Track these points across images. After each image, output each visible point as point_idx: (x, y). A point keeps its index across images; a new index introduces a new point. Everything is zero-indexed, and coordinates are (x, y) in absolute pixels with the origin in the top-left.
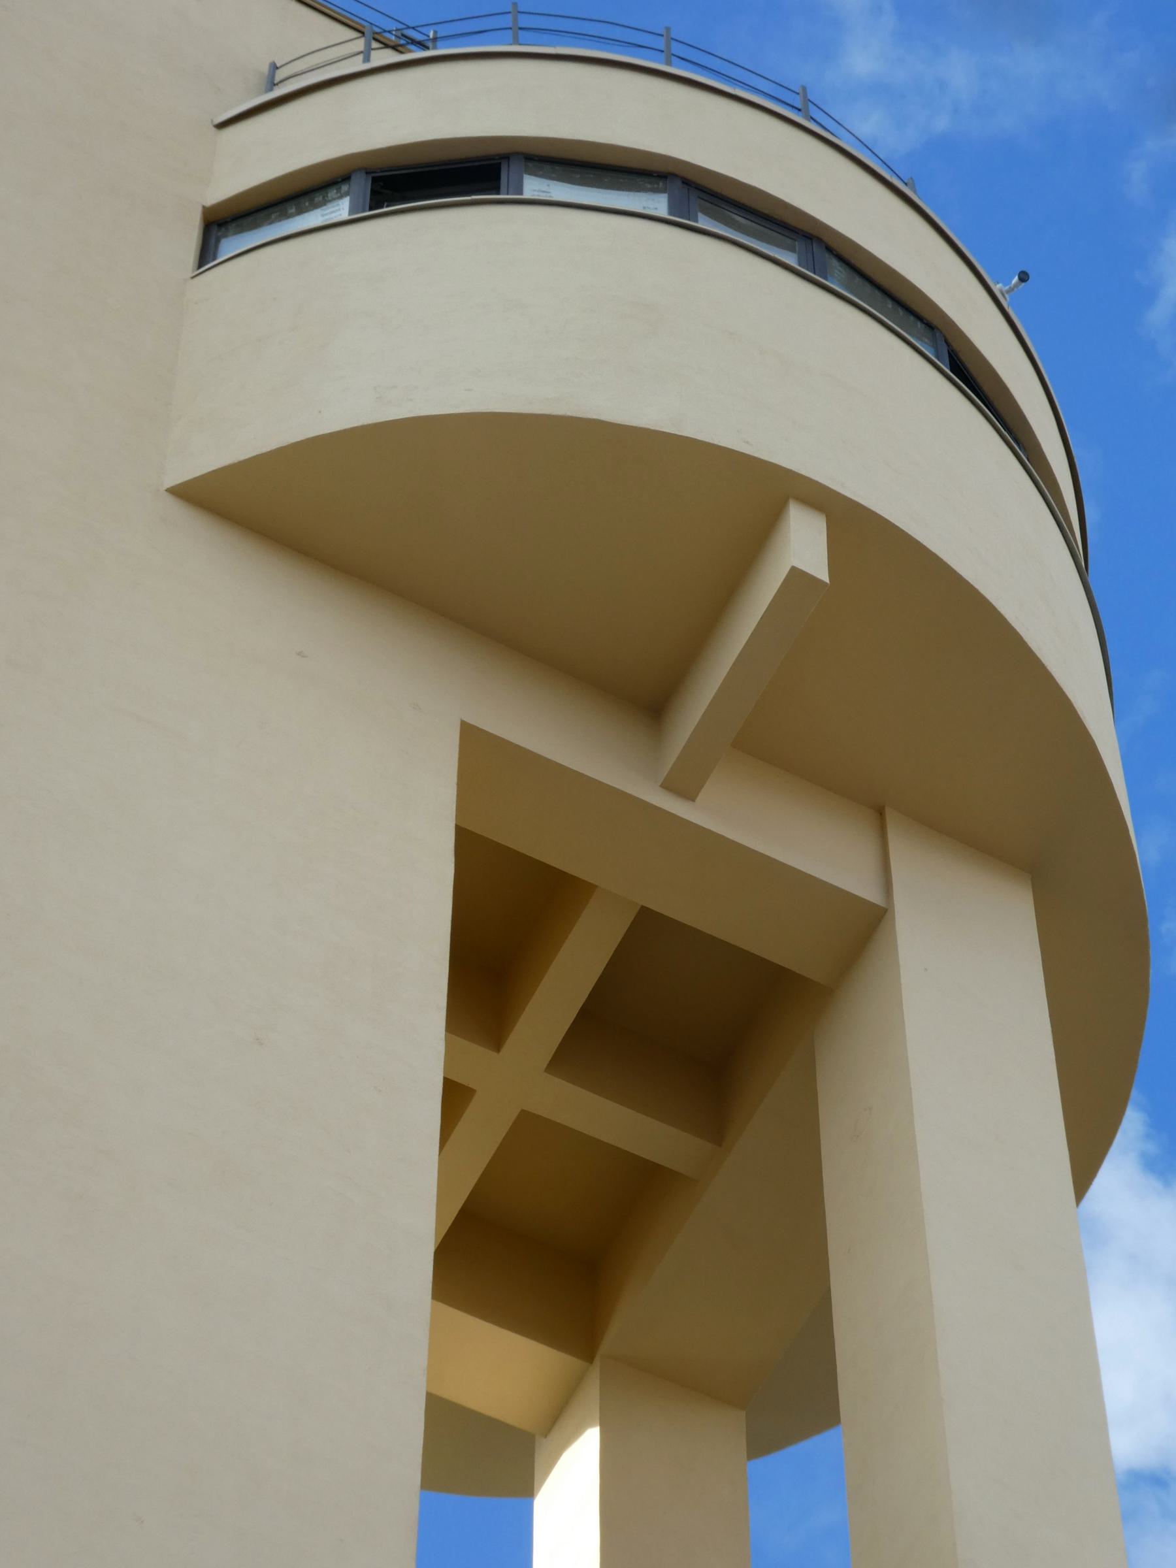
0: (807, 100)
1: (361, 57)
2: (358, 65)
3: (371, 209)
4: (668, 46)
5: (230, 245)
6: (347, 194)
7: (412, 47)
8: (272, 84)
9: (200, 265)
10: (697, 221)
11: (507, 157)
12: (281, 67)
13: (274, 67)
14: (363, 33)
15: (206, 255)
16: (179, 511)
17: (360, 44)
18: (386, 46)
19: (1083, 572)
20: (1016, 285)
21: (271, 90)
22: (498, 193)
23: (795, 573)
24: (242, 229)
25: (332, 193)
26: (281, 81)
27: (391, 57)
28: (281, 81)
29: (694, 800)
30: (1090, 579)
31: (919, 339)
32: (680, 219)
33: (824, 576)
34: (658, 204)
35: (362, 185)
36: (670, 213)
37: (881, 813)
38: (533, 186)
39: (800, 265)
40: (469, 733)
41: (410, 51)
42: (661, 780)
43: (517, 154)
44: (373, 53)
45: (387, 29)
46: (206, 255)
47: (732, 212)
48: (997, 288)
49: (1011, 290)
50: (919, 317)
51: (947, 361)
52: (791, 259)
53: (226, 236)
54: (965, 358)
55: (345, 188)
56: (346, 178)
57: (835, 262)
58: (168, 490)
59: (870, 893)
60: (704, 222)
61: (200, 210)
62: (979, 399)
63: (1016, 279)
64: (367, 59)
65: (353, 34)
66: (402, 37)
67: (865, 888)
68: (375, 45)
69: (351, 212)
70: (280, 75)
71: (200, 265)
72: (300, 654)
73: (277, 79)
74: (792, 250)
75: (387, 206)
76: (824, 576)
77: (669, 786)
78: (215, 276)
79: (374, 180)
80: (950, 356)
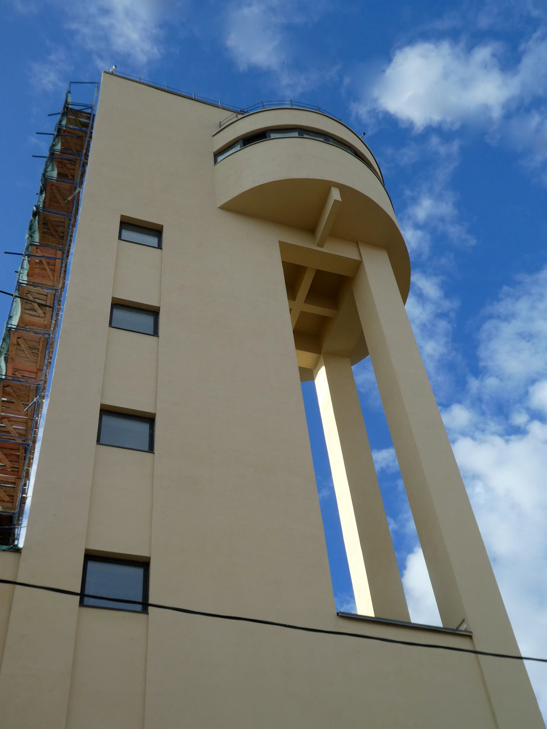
0: (319, 108)
1: (236, 117)
2: (235, 119)
3: (244, 146)
4: (292, 103)
5: (220, 159)
6: (239, 144)
7: (245, 113)
8: (221, 126)
9: (215, 164)
10: (304, 136)
11: (267, 131)
12: (222, 122)
13: (220, 123)
14: (235, 113)
15: (216, 162)
16: (221, 211)
17: (235, 115)
18: (240, 114)
19: (384, 186)
20: (363, 136)
21: (221, 127)
22: (266, 138)
23: (335, 200)
24: (221, 155)
25: (236, 145)
26: (222, 125)
27: (240, 116)
28: (222, 125)
29: (323, 247)
30: (385, 187)
31: (348, 150)
32: (301, 136)
33: (341, 201)
34: (296, 134)
35: (241, 142)
36: (299, 136)
37: (357, 243)
38: (273, 136)
39: (324, 140)
40: (281, 243)
41: (245, 114)
42: (317, 244)
43: (268, 130)
44: (238, 116)
45: (244, 109)
46: (216, 162)
47: (226, 122)
48: (360, 137)
49: (362, 137)
50: (347, 146)
51: (354, 153)
52: (322, 140)
53: (218, 157)
54: (357, 152)
55: (238, 143)
56: (238, 141)
57: (330, 139)
58: (219, 208)
59: (358, 258)
60: (305, 136)
61: (213, 153)
62: (358, 157)
63: (363, 135)
64: (237, 118)
65: (233, 113)
66: (75, 160)
67: (357, 258)
68: (238, 114)
69: (240, 147)
70: (222, 124)
71: (215, 164)
72: (247, 234)
73: (221, 125)
74: (322, 138)
75: (247, 145)
76: (341, 201)
77: (318, 246)
78: (218, 165)
79: (243, 140)
80: (354, 152)
